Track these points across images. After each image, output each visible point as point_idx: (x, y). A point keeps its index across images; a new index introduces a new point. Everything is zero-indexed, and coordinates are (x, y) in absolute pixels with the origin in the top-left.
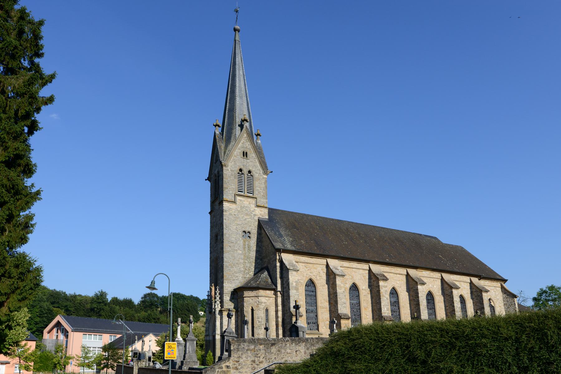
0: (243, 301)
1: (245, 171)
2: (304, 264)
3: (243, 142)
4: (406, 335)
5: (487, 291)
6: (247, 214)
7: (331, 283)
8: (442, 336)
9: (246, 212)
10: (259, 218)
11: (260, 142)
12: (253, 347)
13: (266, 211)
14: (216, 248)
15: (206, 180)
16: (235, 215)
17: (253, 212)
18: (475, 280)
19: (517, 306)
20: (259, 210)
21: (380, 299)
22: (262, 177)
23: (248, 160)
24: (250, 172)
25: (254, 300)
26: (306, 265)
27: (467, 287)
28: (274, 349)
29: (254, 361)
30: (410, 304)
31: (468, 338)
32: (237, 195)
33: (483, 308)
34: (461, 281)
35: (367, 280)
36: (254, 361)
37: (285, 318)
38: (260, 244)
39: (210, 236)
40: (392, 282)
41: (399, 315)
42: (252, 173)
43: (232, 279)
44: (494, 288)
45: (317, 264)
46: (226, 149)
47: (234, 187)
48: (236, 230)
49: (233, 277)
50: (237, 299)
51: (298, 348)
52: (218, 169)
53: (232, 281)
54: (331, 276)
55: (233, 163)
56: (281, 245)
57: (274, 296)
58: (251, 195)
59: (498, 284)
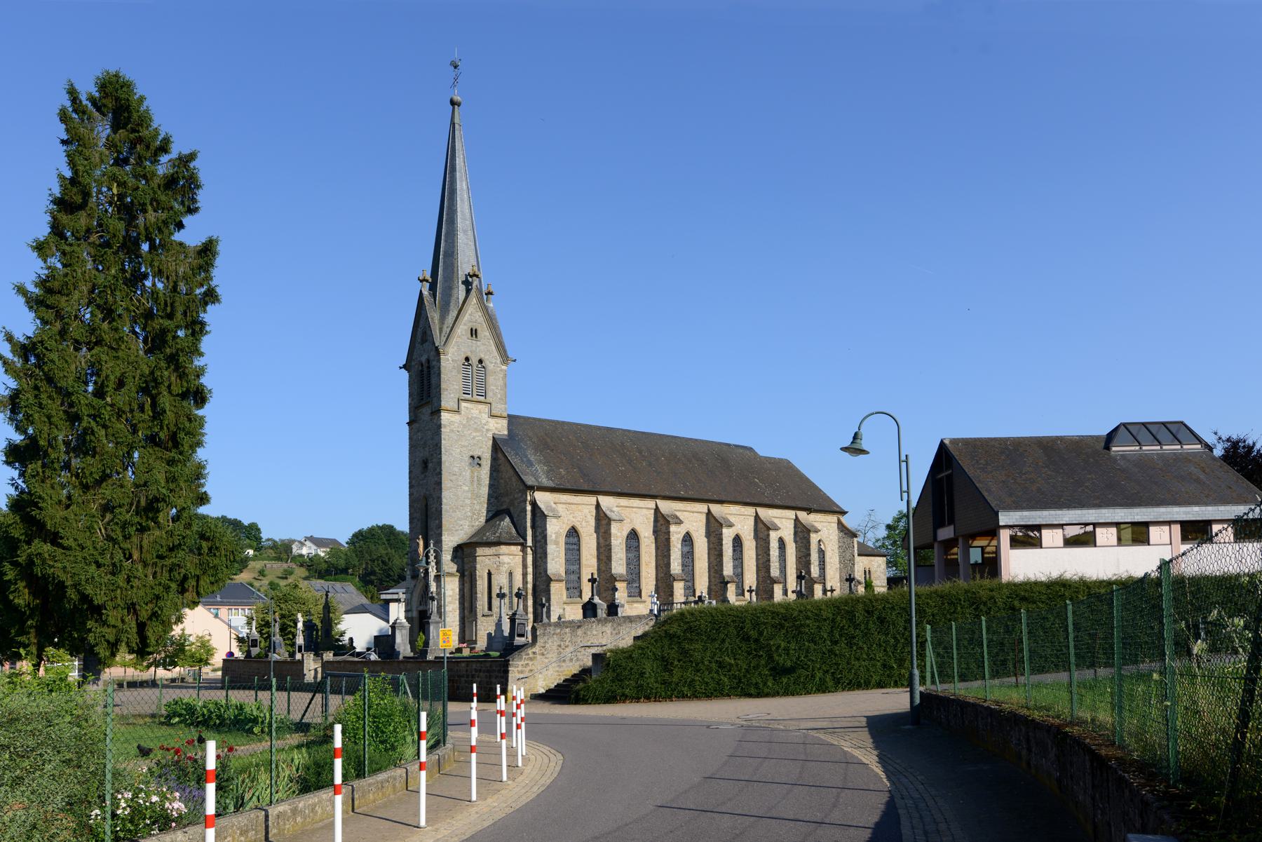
0: (475, 561)
1: (474, 361)
2: (564, 506)
4: (741, 618)
5: (817, 531)
6: (476, 430)
7: (603, 531)
8: (772, 618)
9: (475, 426)
10: (494, 434)
11: (491, 305)
12: (559, 631)
13: (504, 423)
15: (401, 368)
18: (802, 515)
21: (670, 550)
24: (481, 361)
27: (791, 525)
28: (580, 632)
29: (560, 646)
30: (709, 554)
31: (795, 619)
33: (809, 555)
35: (652, 524)
36: (560, 646)
37: (538, 583)
38: (495, 474)
41: (693, 570)
46: (443, 323)
50: (463, 559)
51: (604, 629)
54: (603, 522)
55: (455, 348)
56: (533, 479)
57: (521, 553)
58: (482, 399)
59: (833, 519)
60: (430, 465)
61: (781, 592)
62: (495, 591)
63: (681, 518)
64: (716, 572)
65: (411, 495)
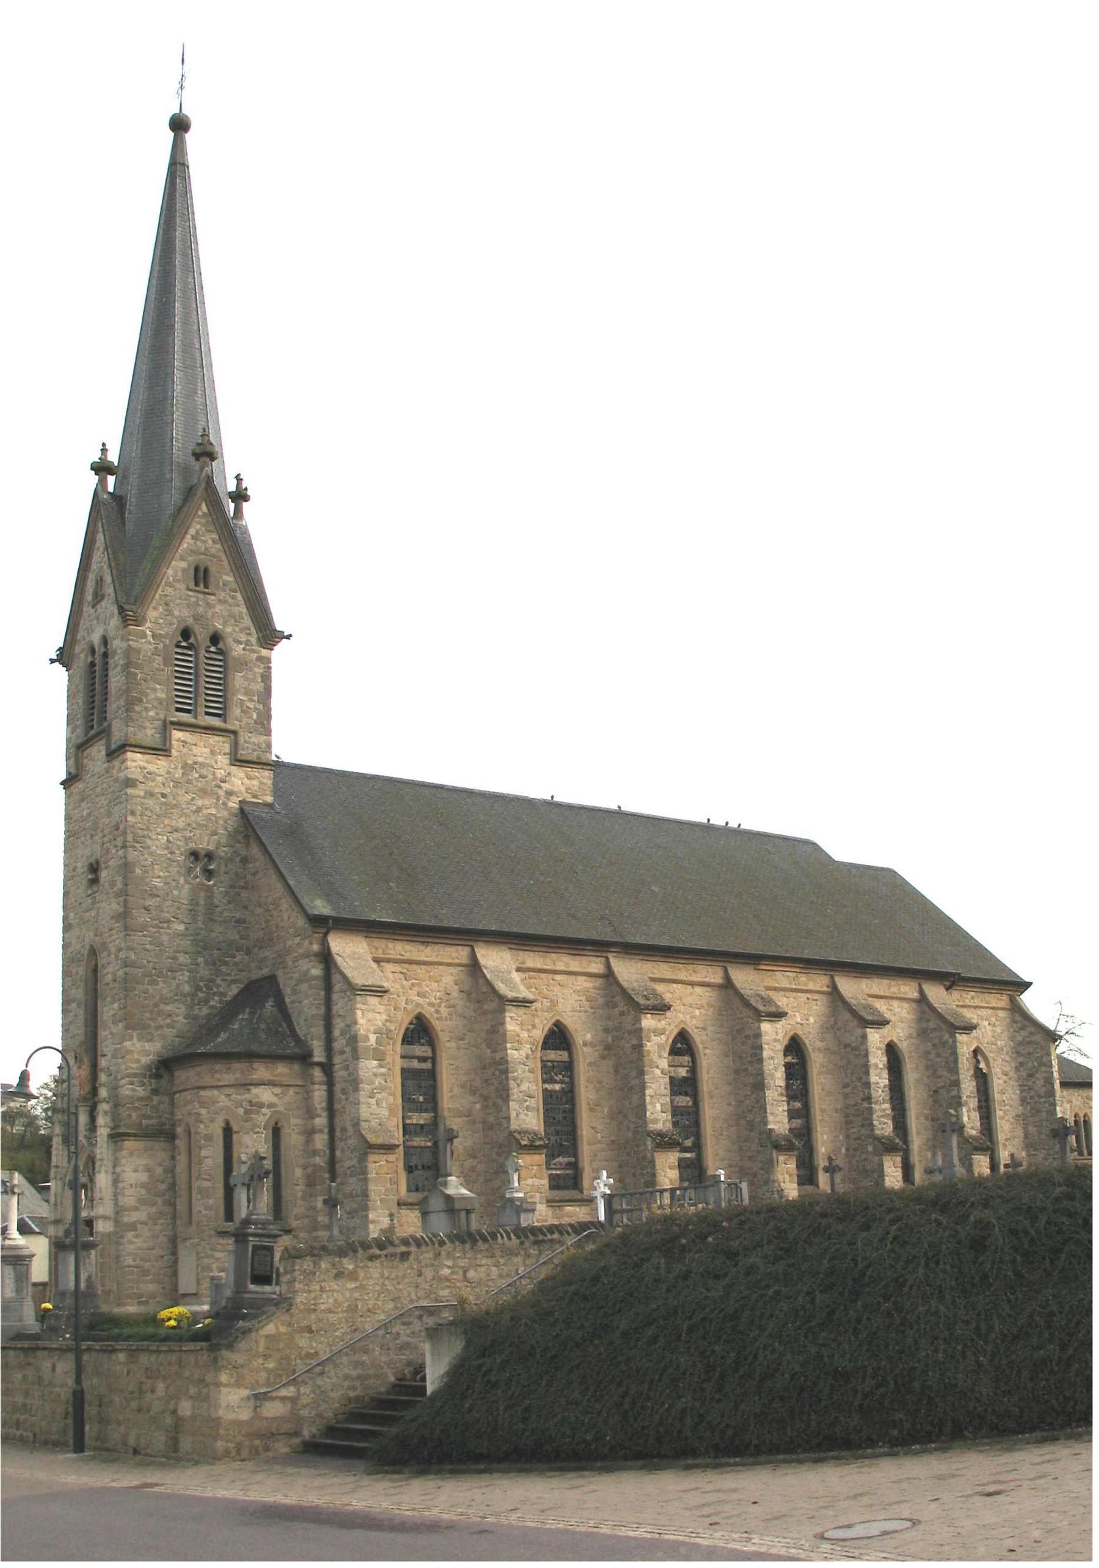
1: (201, 636)
2: (397, 968)
3: (197, 533)
6: (204, 792)
14: (93, 913)
15: (52, 661)
16: (164, 796)
17: (222, 784)
18: (936, 993)
19: (1055, 1068)
20: (242, 775)
22: (255, 655)
23: (213, 597)
24: (215, 639)
25: (234, 1096)
26: (405, 971)
32: (172, 723)
34: (892, 998)
39: (66, 866)
40: (679, 1014)
42: (225, 645)
43: (153, 1024)
44: (990, 1011)
45: (441, 964)
47: (164, 696)
48: (168, 848)
49: (155, 1016)
52: (106, 630)
53: (153, 1031)
59: (1001, 1000)
60: (104, 874)
61: (899, 1174)
62: (241, 1170)
63: (667, 997)
64: (751, 1126)
65: (65, 946)
